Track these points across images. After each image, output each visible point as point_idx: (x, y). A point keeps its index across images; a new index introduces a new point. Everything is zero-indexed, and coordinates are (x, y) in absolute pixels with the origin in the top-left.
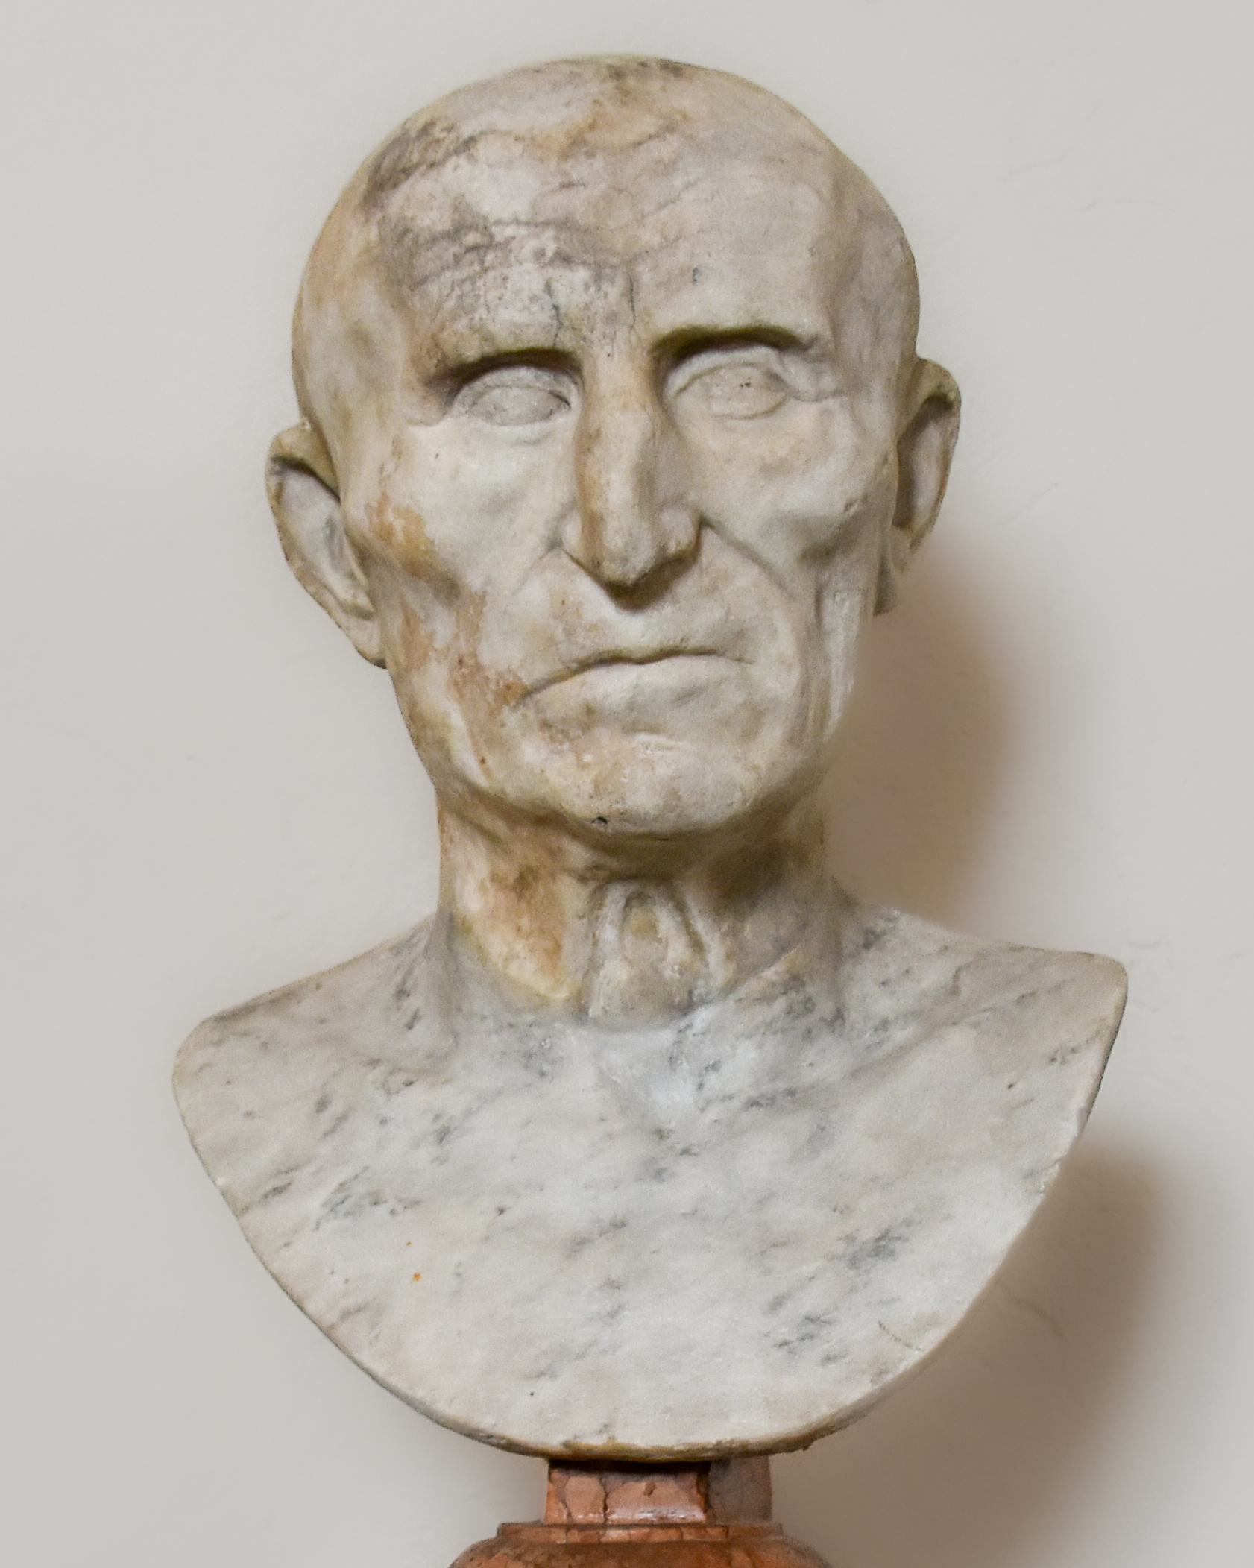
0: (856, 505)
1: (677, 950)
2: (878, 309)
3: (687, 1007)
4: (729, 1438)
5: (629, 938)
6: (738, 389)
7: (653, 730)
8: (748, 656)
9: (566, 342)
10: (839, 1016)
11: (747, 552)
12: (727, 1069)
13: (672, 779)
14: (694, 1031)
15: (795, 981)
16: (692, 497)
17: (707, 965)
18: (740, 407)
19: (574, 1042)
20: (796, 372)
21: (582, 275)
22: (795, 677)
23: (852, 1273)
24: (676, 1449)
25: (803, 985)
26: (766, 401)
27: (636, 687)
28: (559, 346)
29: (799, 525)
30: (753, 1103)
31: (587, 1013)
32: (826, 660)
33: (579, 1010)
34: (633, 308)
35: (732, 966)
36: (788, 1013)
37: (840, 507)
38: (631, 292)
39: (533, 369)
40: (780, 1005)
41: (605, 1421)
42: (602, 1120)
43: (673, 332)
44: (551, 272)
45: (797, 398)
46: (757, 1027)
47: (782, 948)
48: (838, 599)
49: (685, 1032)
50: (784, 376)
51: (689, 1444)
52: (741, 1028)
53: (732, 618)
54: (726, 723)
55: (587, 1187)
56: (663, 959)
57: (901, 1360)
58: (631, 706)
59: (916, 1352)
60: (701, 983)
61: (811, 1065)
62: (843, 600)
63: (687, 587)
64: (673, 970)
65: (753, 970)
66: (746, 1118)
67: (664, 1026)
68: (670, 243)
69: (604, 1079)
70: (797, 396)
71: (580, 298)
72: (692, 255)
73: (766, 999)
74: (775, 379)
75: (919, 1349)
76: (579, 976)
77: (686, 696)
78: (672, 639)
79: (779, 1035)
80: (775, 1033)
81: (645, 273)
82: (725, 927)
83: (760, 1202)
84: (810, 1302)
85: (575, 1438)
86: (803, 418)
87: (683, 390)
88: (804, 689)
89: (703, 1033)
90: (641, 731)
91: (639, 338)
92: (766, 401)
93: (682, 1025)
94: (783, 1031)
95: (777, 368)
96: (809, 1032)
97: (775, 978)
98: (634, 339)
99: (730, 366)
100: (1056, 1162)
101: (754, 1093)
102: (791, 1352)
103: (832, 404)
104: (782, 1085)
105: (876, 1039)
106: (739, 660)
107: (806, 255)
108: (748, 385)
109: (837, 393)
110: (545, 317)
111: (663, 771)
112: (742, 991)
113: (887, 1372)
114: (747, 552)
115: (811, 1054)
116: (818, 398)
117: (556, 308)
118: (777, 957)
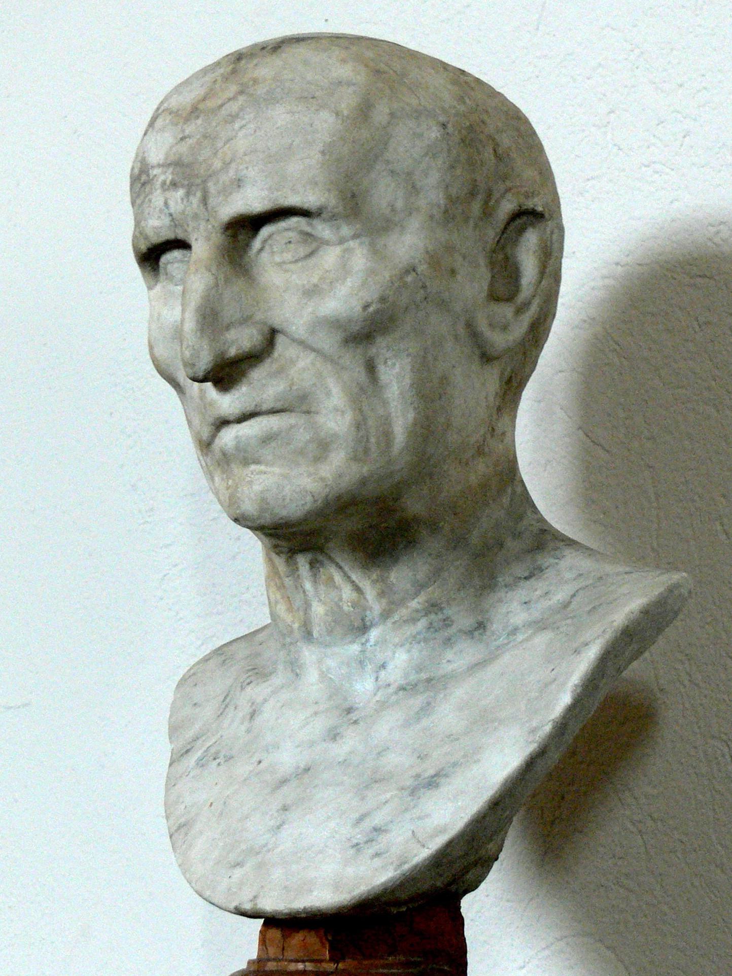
0: (374, 306)
1: (347, 593)
3: (364, 629)
4: (309, 905)
5: (322, 588)
6: (284, 246)
7: (257, 462)
8: (313, 409)
9: (181, 235)
10: (481, 626)
11: (302, 343)
12: (390, 667)
13: (262, 492)
15: (433, 607)
16: (259, 316)
18: (288, 256)
19: (309, 654)
20: (322, 229)
21: (181, 192)
22: (349, 417)
23: (409, 799)
25: (441, 609)
26: (302, 251)
27: (237, 437)
28: (179, 238)
29: (335, 324)
30: (402, 688)
31: (312, 635)
32: (385, 403)
33: (308, 635)
34: (206, 209)
35: (384, 601)
37: (359, 308)
38: (204, 200)
39: (181, 251)
40: (422, 624)
41: (254, 894)
42: (316, 703)
43: (230, 220)
44: (168, 194)
45: (328, 245)
46: (407, 639)
47: (420, 587)
48: (389, 363)
49: (365, 644)
51: (291, 909)
52: (397, 640)
53: (295, 388)
54: (301, 452)
56: (341, 599)
57: (416, 856)
59: (426, 850)
60: (368, 613)
61: (449, 661)
62: (394, 364)
63: (257, 374)
64: (348, 606)
65: (402, 603)
68: (226, 165)
69: (323, 676)
70: (327, 243)
71: (180, 207)
72: (237, 170)
73: (413, 620)
74: (307, 236)
75: (428, 848)
76: (301, 613)
77: (267, 439)
78: (250, 408)
79: (422, 644)
80: (419, 643)
81: (212, 187)
82: (374, 576)
84: (378, 819)
85: (240, 904)
86: (330, 257)
87: (261, 250)
88: (359, 425)
89: (375, 645)
90: (251, 463)
91: (213, 226)
92: (302, 251)
93: (364, 640)
94: (426, 640)
95: (308, 229)
97: (419, 607)
98: (210, 226)
99: (279, 232)
100: (549, 721)
101: (402, 682)
102: (358, 850)
103: (352, 244)
104: (423, 676)
105: (506, 641)
106: (308, 412)
108: (290, 242)
109: (355, 237)
110: (167, 221)
111: (257, 488)
112: (396, 617)
113: (405, 863)
114: (302, 343)
115: (449, 654)
116: (342, 241)
117: (171, 215)
118: (416, 594)
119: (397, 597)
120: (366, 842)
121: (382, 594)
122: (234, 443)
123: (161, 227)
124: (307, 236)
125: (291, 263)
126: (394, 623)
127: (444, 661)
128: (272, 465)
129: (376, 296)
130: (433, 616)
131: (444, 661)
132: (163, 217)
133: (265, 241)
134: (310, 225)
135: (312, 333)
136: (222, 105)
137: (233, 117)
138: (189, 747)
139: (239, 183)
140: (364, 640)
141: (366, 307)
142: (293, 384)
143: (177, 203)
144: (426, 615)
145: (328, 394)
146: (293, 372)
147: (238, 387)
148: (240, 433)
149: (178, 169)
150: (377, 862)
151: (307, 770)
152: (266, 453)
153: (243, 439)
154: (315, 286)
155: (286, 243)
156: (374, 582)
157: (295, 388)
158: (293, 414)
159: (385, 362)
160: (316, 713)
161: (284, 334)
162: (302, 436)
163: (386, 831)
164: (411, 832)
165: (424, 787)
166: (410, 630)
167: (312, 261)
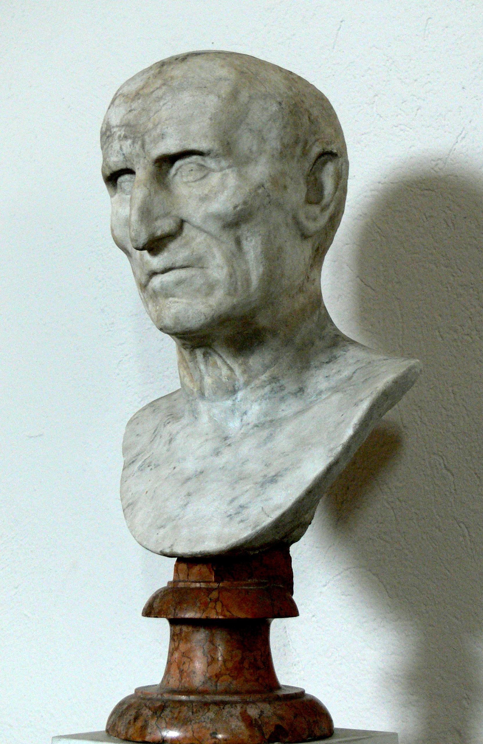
1: (225, 371)
2: (260, 131)
3: (234, 391)
4: (203, 550)
5: (210, 368)
7: (173, 296)
8: (205, 266)
9: (129, 166)
10: (301, 390)
11: (199, 228)
12: (249, 413)
13: (176, 313)
14: (238, 400)
15: (274, 379)
16: (174, 213)
17: (236, 376)
18: (191, 178)
19: (202, 406)
20: (210, 163)
21: (129, 142)
22: (225, 270)
24: (189, 554)
25: (279, 380)
26: (199, 175)
27: (161, 282)
28: (128, 168)
29: (217, 217)
30: (256, 426)
31: (205, 395)
32: (246, 262)
33: (202, 395)
34: (144, 151)
36: (272, 391)
37: (231, 208)
38: (143, 146)
40: (267, 389)
42: (207, 434)
44: (122, 143)
45: (213, 172)
47: (266, 368)
48: (249, 239)
50: (205, 165)
52: (253, 398)
53: (195, 253)
54: (198, 291)
55: (196, 459)
56: (221, 375)
57: (264, 522)
58: (162, 288)
59: (270, 518)
60: (237, 382)
61: (283, 410)
62: (252, 240)
63: (173, 246)
64: (225, 379)
65: (256, 377)
66: (251, 431)
67: (227, 399)
68: (155, 126)
69: (211, 419)
70: (213, 171)
71: (129, 150)
72: (161, 129)
73: (263, 387)
74: (202, 167)
77: (179, 283)
78: (169, 265)
79: (268, 400)
80: (266, 400)
81: (147, 139)
82: (240, 362)
83: (243, 463)
84: (242, 501)
86: (215, 178)
87: (175, 174)
89: (240, 401)
91: (148, 161)
92: (199, 175)
93: (234, 398)
94: (269, 398)
95: (202, 163)
96: (283, 398)
97: (266, 379)
98: (146, 161)
99: (186, 164)
101: (256, 422)
102: (231, 519)
103: (227, 171)
104: (268, 419)
105: (315, 399)
106: (202, 268)
107: (208, 121)
108: (192, 170)
109: (229, 167)
110: (121, 158)
111: (173, 311)
112: (253, 385)
113: (258, 526)
114: (199, 228)
115: (283, 406)
116: (221, 170)
117: (124, 154)
118: (264, 372)
119: (253, 373)
120: (236, 514)
121: (244, 372)
122: (160, 285)
123: (118, 162)
124: (202, 167)
125: (192, 182)
126: (251, 388)
127: (280, 410)
128: (182, 298)
129: (241, 201)
130: (274, 384)
131: (280, 410)
132: (119, 156)
133: (177, 170)
134: (204, 160)
135: (205, 222)
136: (153, 92)
137: (159, 99)
138: (134, 459)
139: (163, 136)
140: (234, 398)
141: (235, 207)
142: (193, 251)
143: (127, 148)
144: (270, 384)
145: (214, 257)
146: (193, 244)
147: (162, 253)
148: (163, 280)
149: (128, 128)
150: (242, 525)
151: (202, 472)
152: (178, 291)
153: (165, 283)
154: (206, 195)
155: (190, 171)
156: (240, 365)
157: (195, 253)
158: (194, 269)
159: (247, 239)
160: (207, 440)
161: (189, 223)
162: (199, 281)
163: (247, 507)
164: (261, 508)
165: (268, 482)
166: (261, 392)
167: (204, 181)
